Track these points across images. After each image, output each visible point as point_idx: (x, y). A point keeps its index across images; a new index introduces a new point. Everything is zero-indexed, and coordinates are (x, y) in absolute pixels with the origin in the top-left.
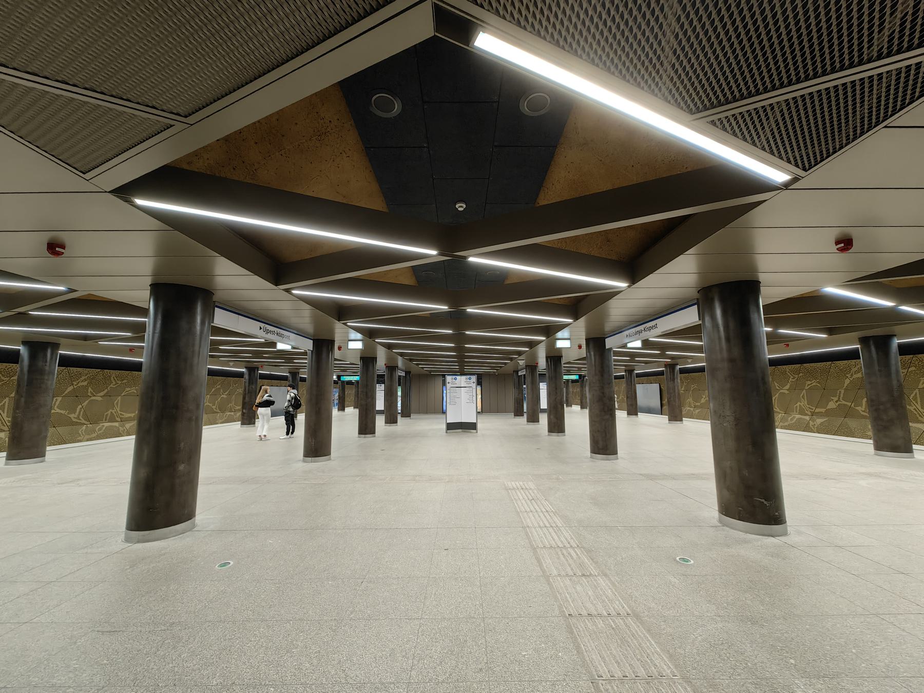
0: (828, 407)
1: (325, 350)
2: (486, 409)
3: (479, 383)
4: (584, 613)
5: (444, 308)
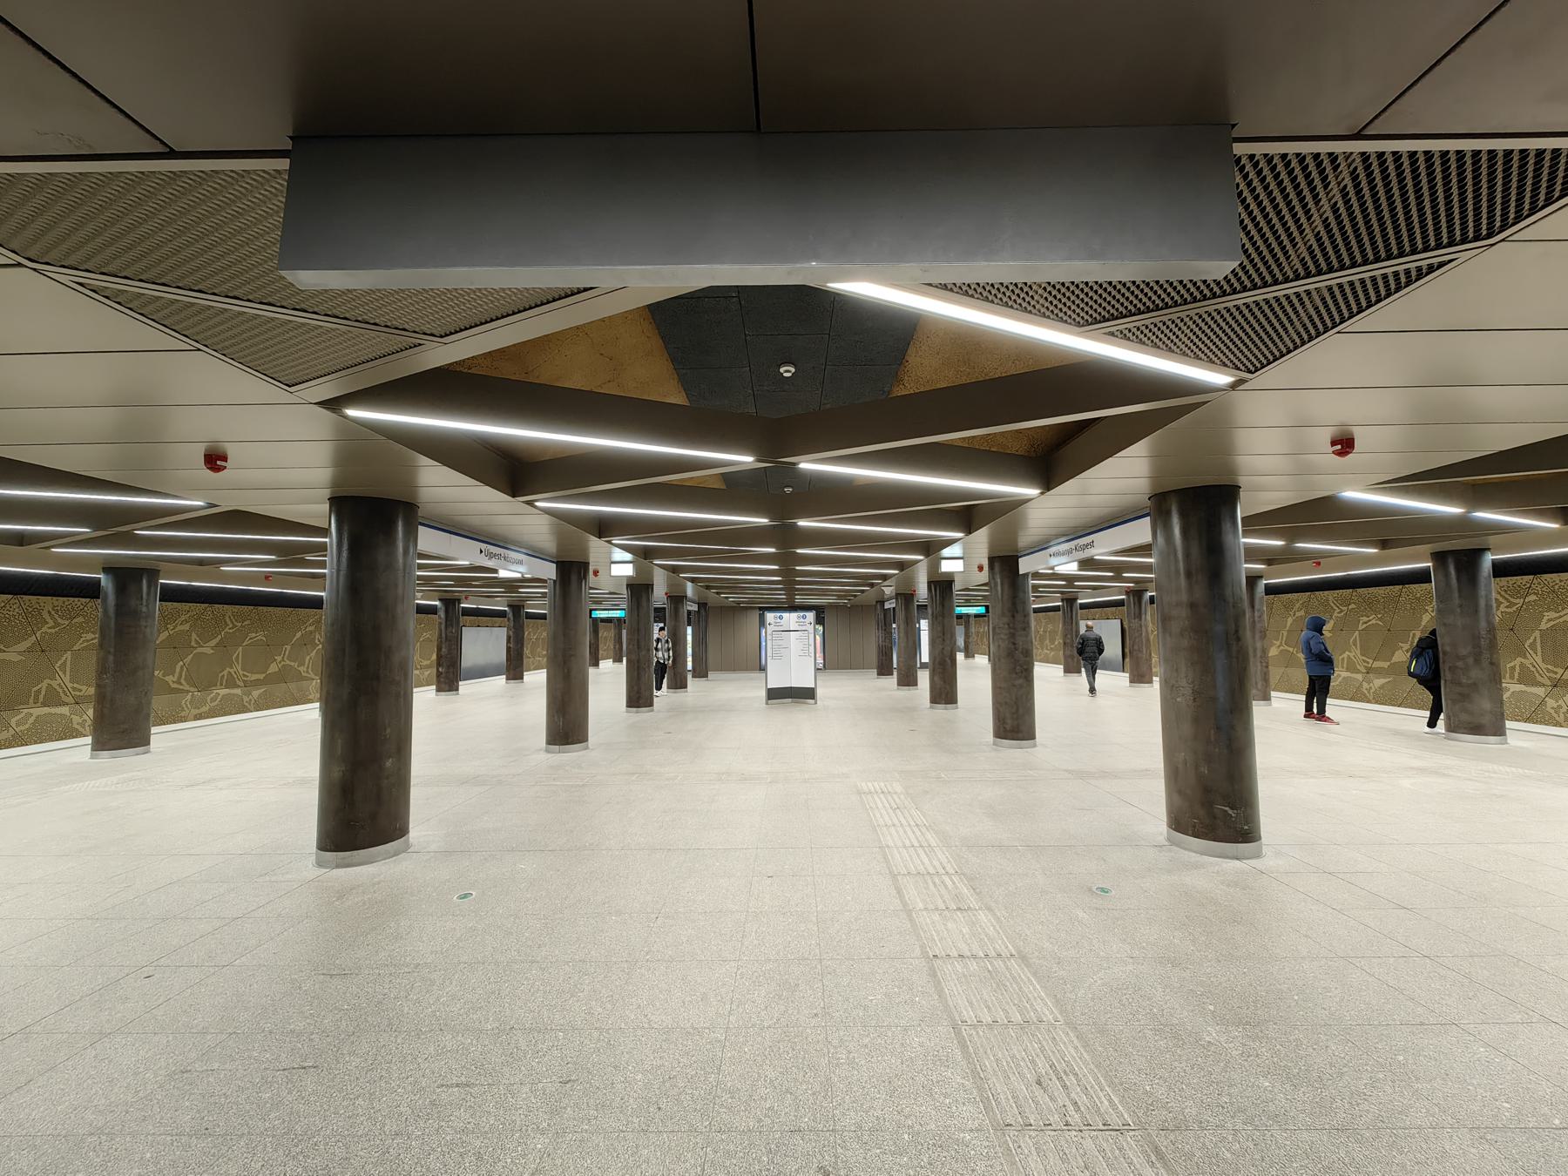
0: (1394, 659)
1: (574, 578)
2: (834, 661)
3: (820, 620)
4: (954, 953)
5: (764, 521)
